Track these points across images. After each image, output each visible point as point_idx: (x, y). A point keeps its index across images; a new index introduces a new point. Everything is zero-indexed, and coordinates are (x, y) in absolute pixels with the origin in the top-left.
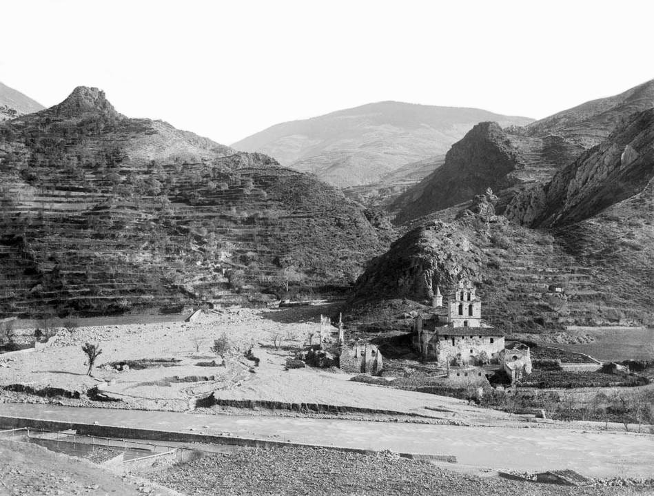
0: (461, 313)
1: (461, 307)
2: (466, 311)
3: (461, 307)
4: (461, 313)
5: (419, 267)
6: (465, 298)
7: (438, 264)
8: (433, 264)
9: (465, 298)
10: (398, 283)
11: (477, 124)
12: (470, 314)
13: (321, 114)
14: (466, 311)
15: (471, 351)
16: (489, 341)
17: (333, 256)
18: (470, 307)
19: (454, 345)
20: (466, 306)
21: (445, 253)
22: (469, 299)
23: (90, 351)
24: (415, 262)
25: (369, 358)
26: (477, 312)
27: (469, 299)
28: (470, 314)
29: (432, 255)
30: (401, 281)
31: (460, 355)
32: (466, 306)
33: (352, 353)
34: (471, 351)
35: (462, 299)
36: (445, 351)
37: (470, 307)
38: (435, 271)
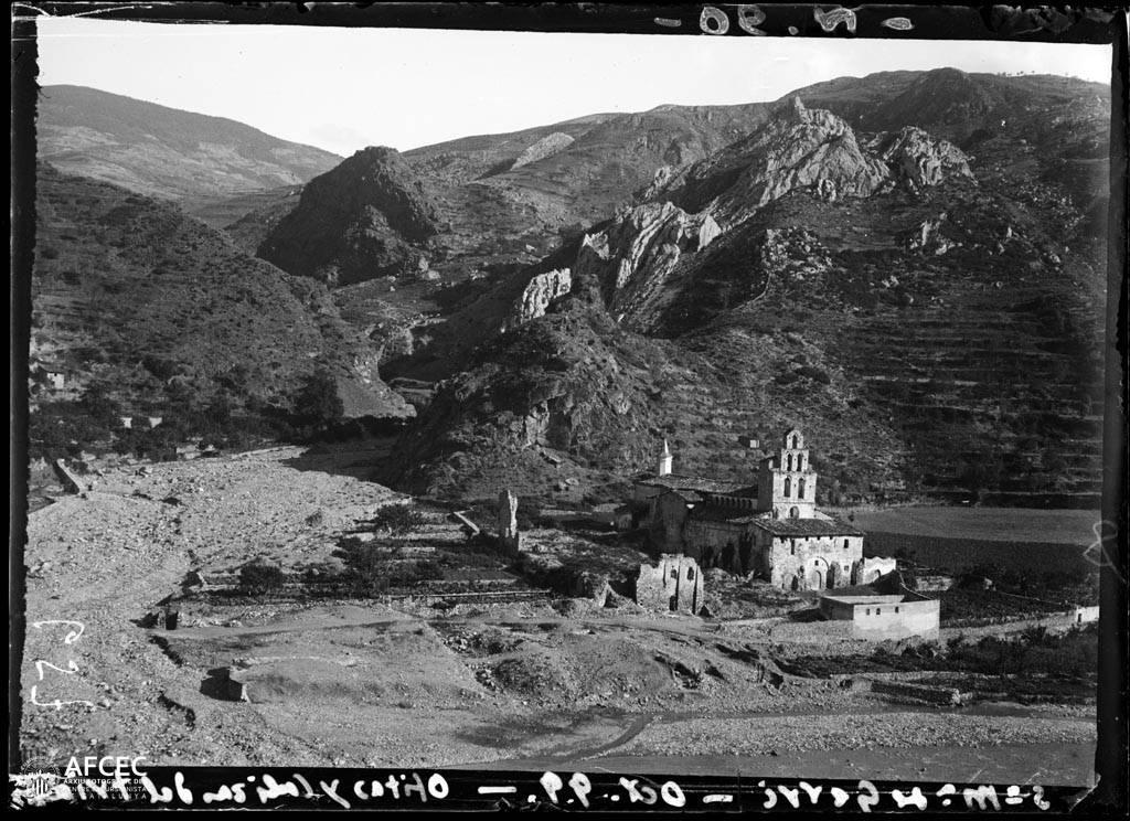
0: (787, 494)
1: (788, 480)
2: (794, 492)
3: (788, 480)
4: (787, 494)
11: (362, 148)
12: (801, 495)
14: (794, 492)
15: (817, 563)
16: (864, 613)
17: (255, 361)
18: (801, 481)
19: (793, 553)
20: (795, 481)
22: (799, 469)
23: (54, 795)
24: (561, 389)
26: (810, 494)
27: (799, 469)
28: (801, 495)
31: (802, 570)
32: (795, 481)
33: (658, 573)
34: (817, 563)
36: (782, 559)
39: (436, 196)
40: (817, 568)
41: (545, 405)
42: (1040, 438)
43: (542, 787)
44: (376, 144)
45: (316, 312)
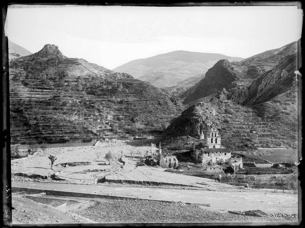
0: (212, 142)
1: (212, 139)
2: (214, 141)
4: (212, 142)
5: (194, 122)
6: (214, 135)
7: (202, 121)
8: (200, 121)
9: (214, 135)
10: (185, 129)
12: (216, 142)
13: (166, 53)
14: (214, 141)
15: (217, 159)
18: (216, 139)
19: (209, 156)
20: (214, 139)
21: (205, 116)
22: (215, 136)
25: (172, 162)
26: (219, 142)
27: (215, 136)
28: (216, 142)
29: (200, 117)
30: (186, 128)
31: (211, 160)
32: (214, 139)
33: (165, 159)
34: (217, 159)
35: (212, 136)
36: (205, 158)
37: (216, 139)
38: (201, 124)
39: (239, 70)
40: (217, 160)
41: (189, 124)
42: (21, 122)
43: (11, 162)
44: (222, 59)
45: (176, 105)
